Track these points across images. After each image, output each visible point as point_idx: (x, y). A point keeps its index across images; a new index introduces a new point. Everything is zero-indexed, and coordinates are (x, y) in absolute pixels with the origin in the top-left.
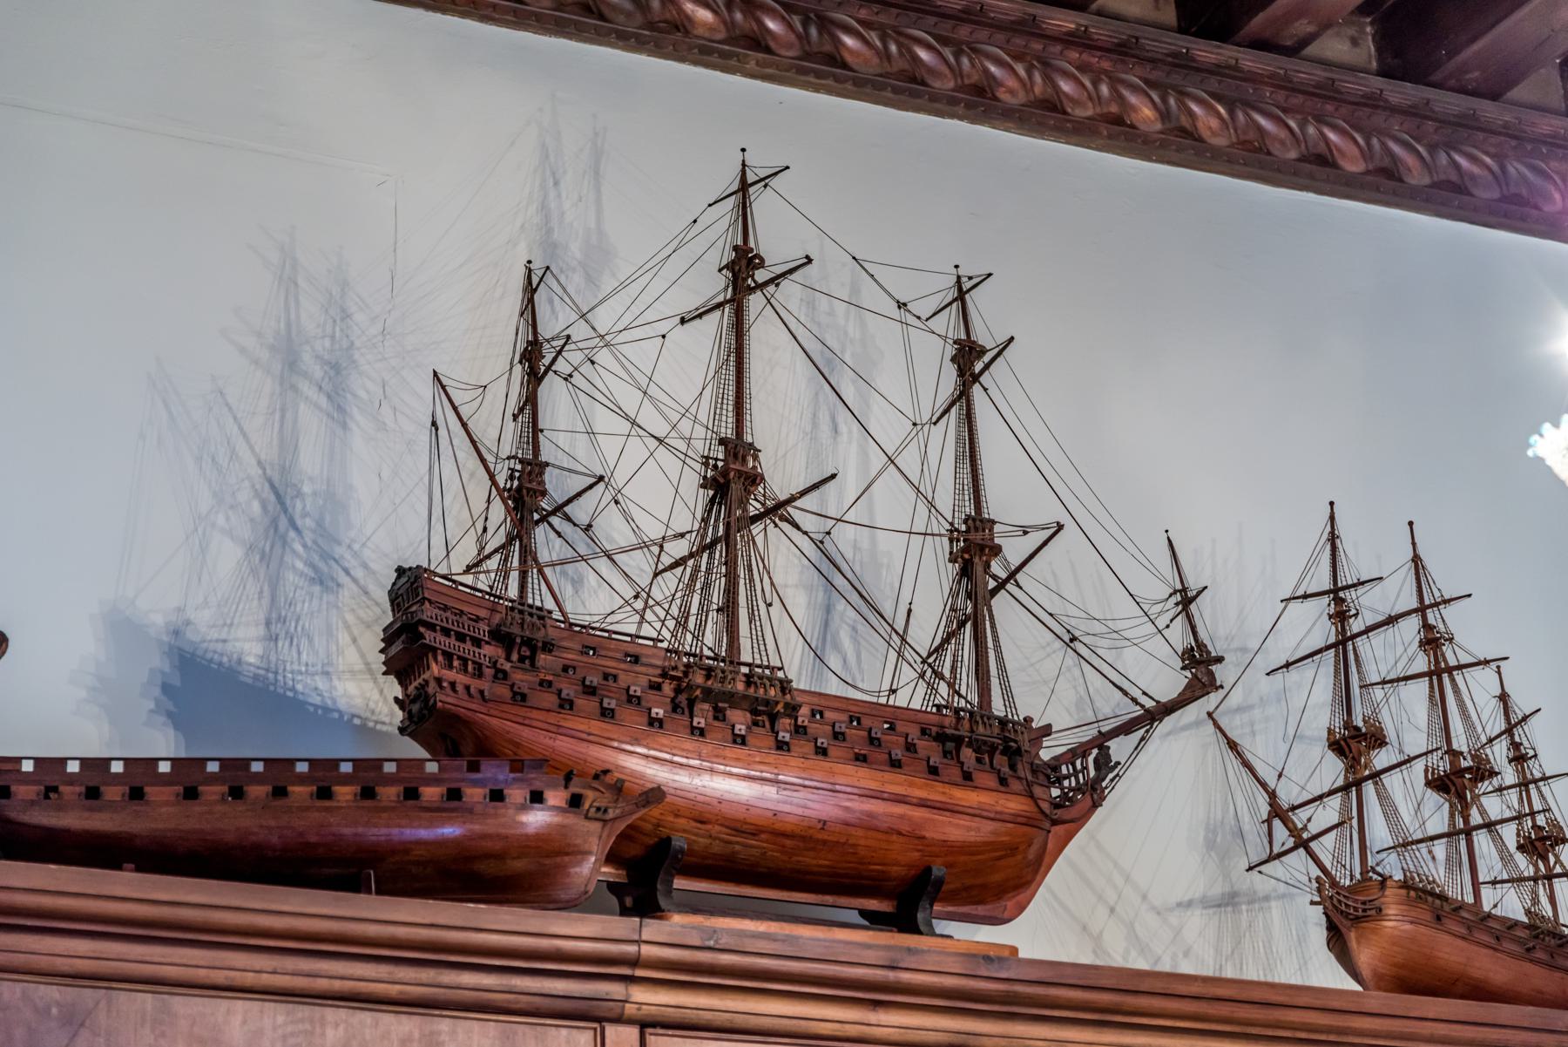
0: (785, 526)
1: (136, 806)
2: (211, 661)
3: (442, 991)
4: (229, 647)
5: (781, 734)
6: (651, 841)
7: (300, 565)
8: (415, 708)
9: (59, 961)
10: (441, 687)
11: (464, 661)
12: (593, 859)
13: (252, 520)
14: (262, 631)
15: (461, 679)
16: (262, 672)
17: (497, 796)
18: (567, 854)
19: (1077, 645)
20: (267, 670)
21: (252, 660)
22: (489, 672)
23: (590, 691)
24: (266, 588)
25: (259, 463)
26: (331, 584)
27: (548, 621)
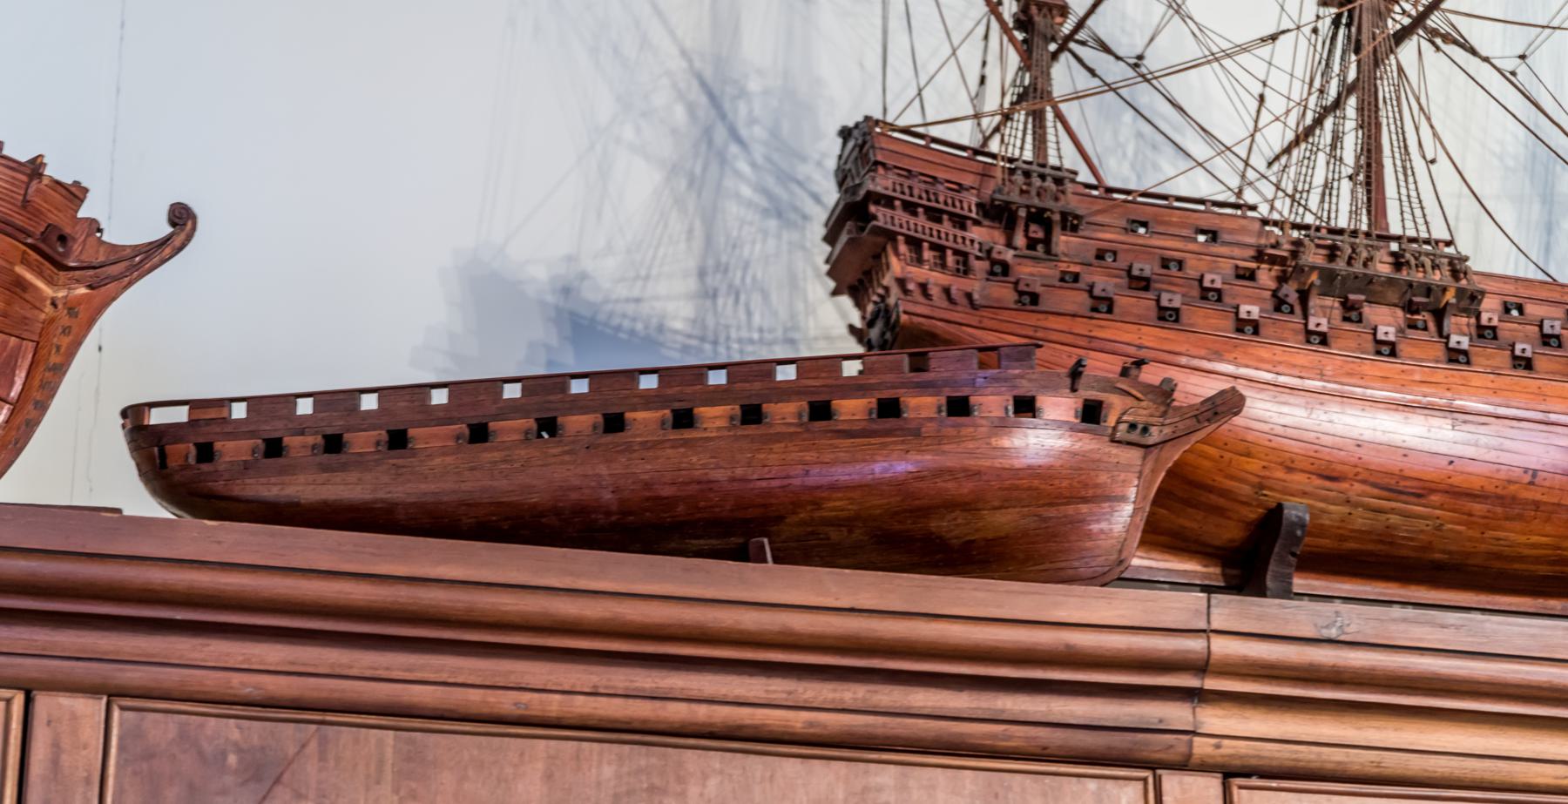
1: (396, 459)
2: (618, 328)
3: (881, 720)
4: (645, 309)
5: (1454, 339)
6: (1253, 514)
7: (746, 191)
8: (874, 333)
9: (236, 679)
10: (906, 291)
11: (939, 249)
12: (1128, 509)
13: (674, 131)
14: (692, 284)
15: (936, 278)
16: (694, 342)
17: (959, 407)
18: (1085, 500)
20: (703, 339)
21: (678, 325)
22: (980, 266)
23: (1141, 284)
24: (698, 225)
25: (684, 53)
26: (793, 216)
27: (1069, 187)
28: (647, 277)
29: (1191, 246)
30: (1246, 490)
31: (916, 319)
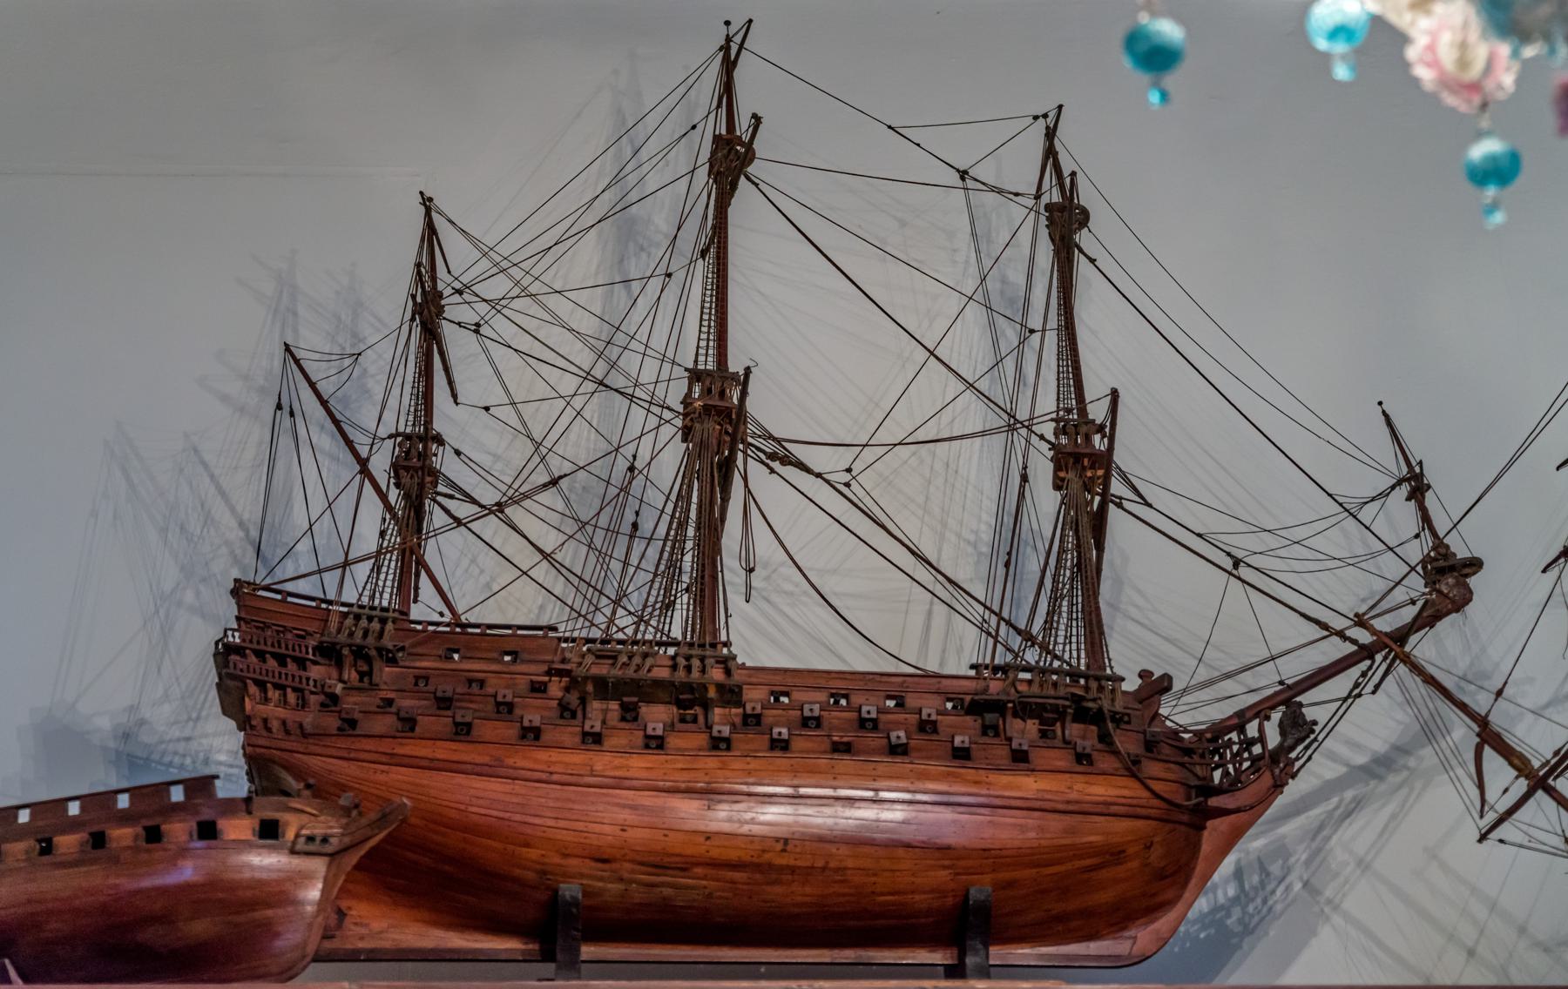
0: (790, 472)
5: (716, 728)
18: (269, 906)
19: (1243, 571)
21: (222, 758)
23: (444, 703)
25: (241, 524)
28: (198, 718)
29: (494, 667)
30: (530, 876)
31: (258, 750)
